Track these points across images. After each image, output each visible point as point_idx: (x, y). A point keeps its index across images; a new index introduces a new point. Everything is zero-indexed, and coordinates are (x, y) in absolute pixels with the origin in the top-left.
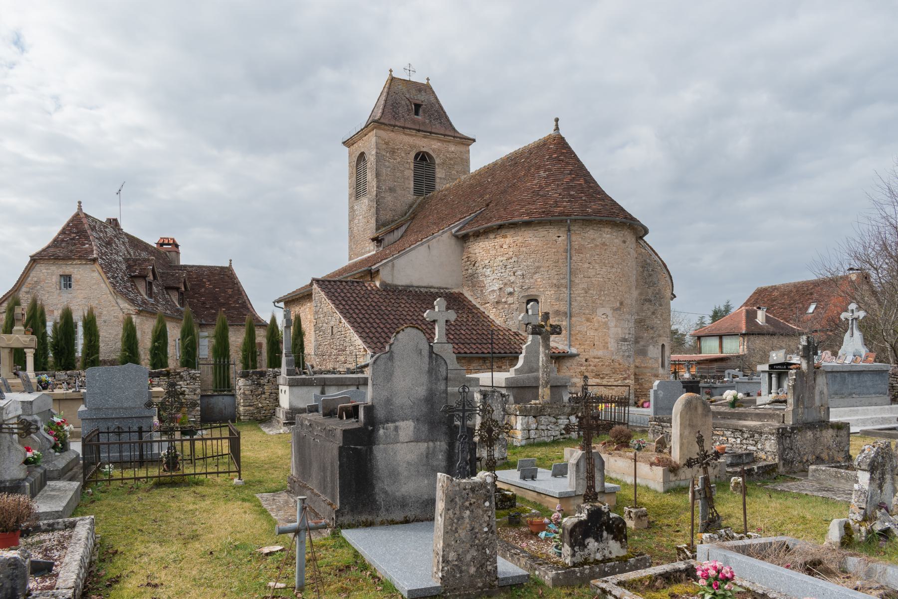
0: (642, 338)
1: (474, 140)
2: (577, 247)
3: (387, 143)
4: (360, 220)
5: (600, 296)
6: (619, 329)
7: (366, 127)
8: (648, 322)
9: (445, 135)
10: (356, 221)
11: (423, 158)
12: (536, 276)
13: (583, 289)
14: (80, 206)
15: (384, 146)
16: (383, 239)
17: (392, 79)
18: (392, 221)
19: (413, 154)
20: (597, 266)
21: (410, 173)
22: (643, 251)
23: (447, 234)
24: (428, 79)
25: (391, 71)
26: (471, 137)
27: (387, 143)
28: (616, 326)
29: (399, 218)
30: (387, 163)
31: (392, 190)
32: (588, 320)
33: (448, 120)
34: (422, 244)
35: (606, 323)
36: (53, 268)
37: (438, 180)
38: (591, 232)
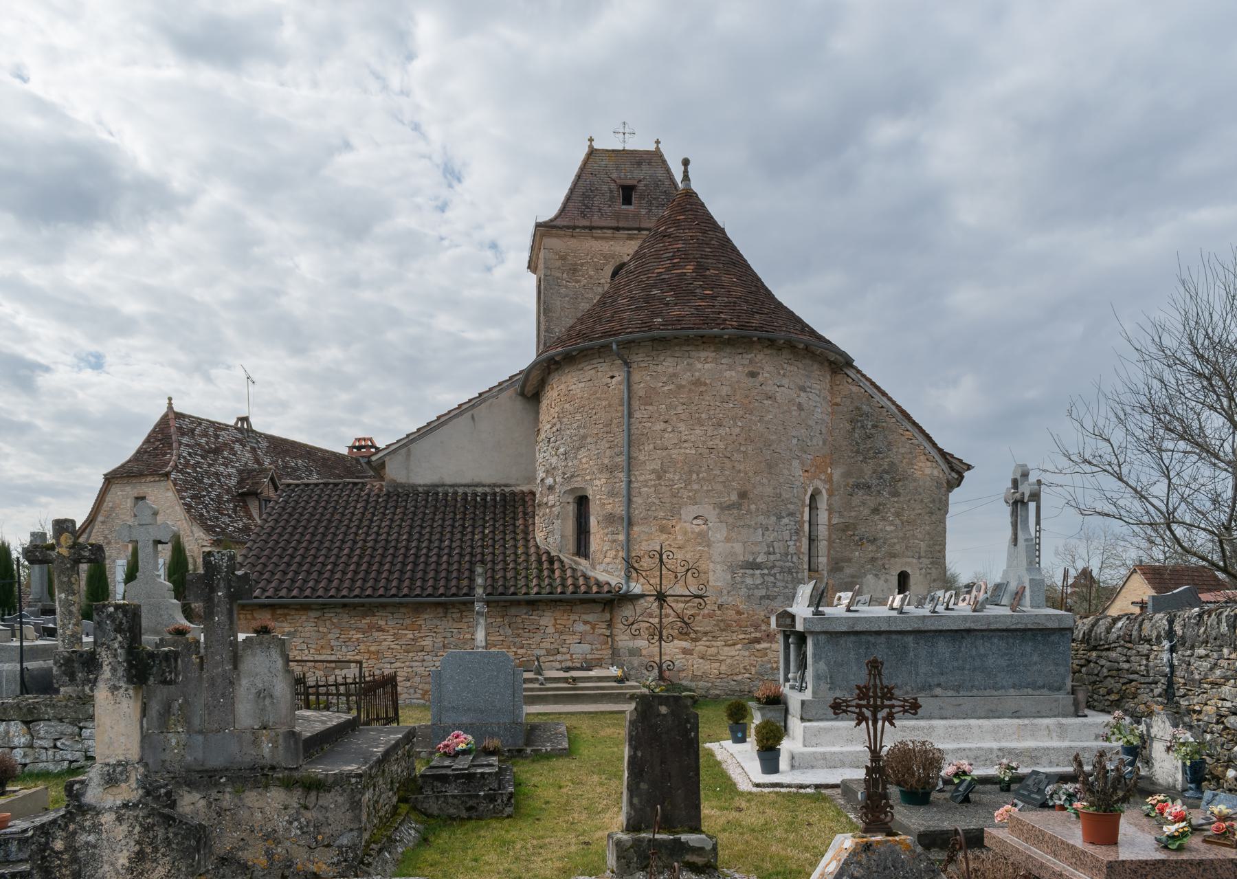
0: (849, 560)
2: (642, 393)
5: (688, 483)
6: (738, 548)
8: (862, 529)
12: (582, 453)
13: (654, 471)
14: (170, 404)
15: (559, 263)
19: (609, 270)
20: (682, 427)
22: (855, 389)
27: (563, 258)
28: (728, 540)
30: (563, 290)
32: (663, 529)
35: (702, 535)
36: (128, 488)
38: (670, 362)
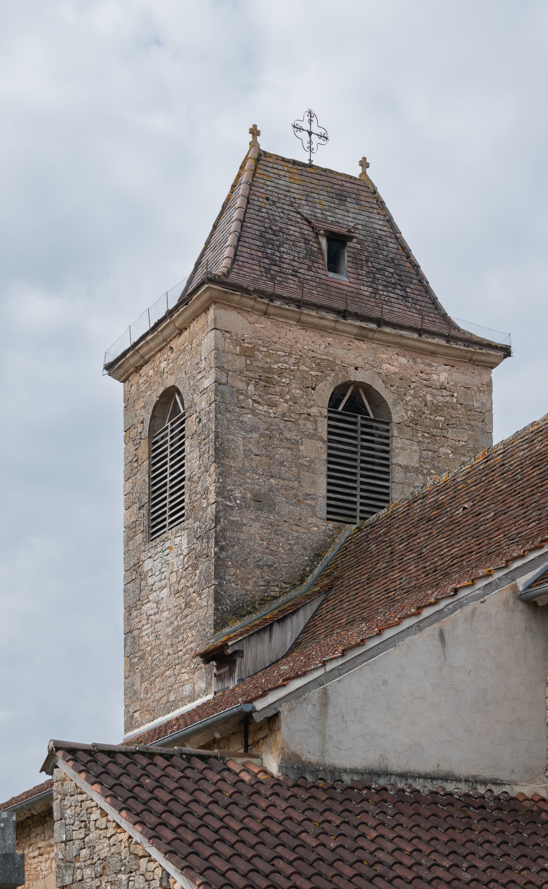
1: (506, 351)
3: (248, 353)
4: (162, 601)
7: (185, 300)
9: (420, 332)
10: (149, 608)
11: (355, 408)
15: (240, 363)
16: (238, 653)
17: (260, 161)
18: (264, 601)
19: (325, 391)
21: (315, 451)
23: (498, 598)
24: (364, 164)
25: (255, 132)
26: (498, 340)
27: (248, 353)
29: (283, 592)
31: (261, 501)
33: (427, 290)
34: (419, 627)
37: (397, 475)
